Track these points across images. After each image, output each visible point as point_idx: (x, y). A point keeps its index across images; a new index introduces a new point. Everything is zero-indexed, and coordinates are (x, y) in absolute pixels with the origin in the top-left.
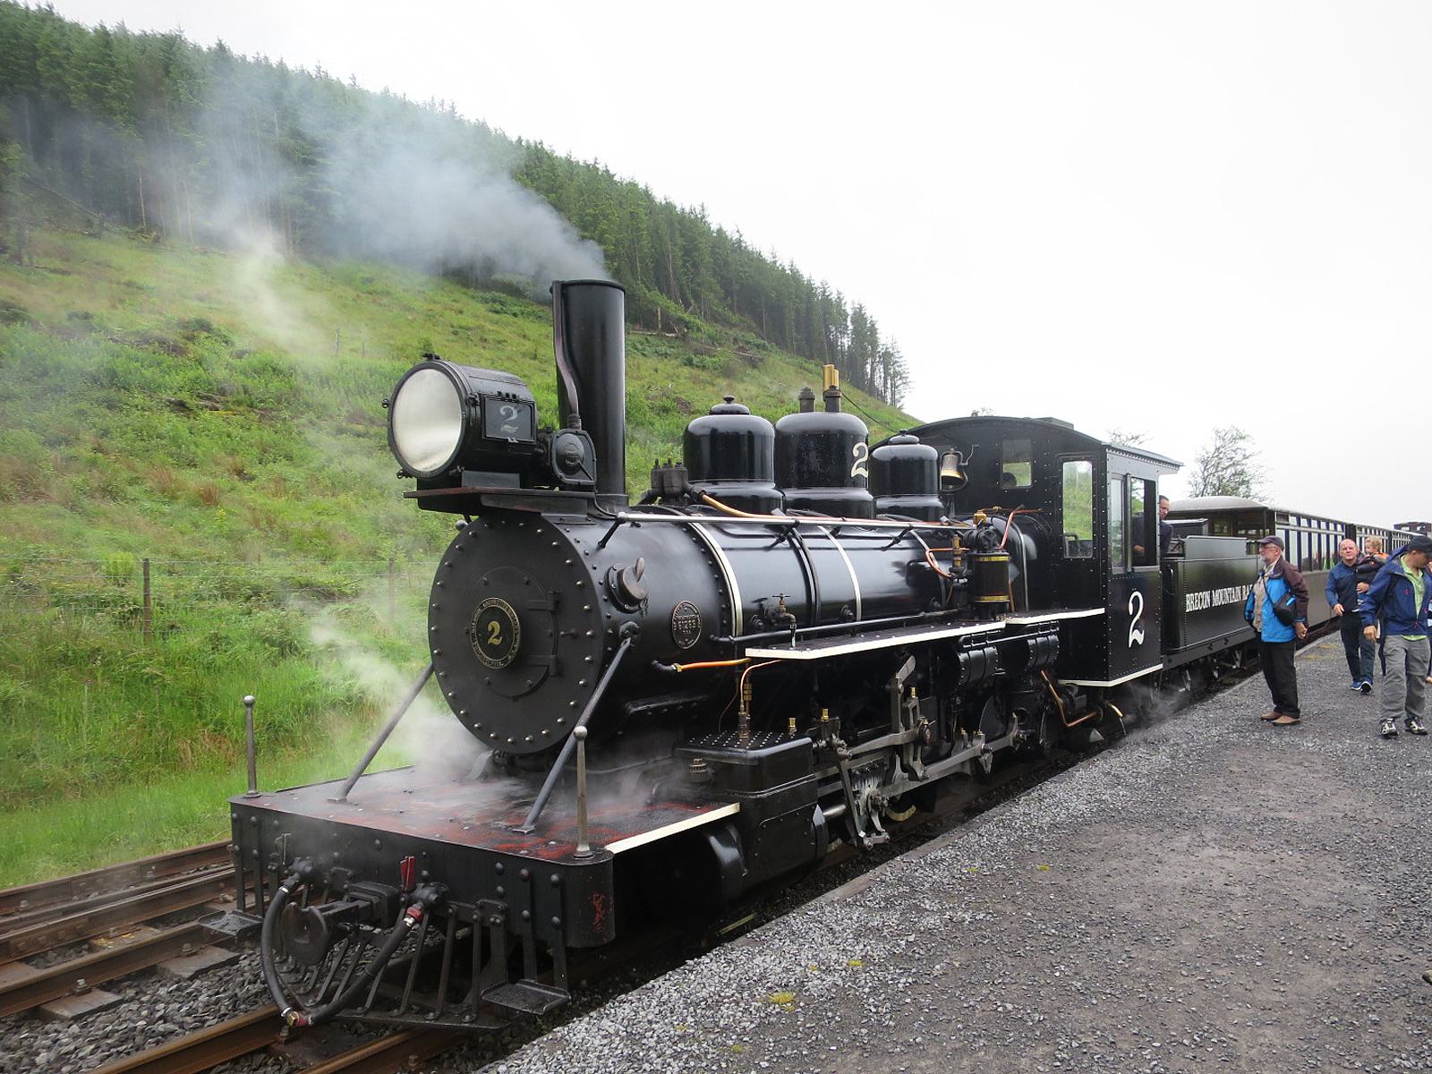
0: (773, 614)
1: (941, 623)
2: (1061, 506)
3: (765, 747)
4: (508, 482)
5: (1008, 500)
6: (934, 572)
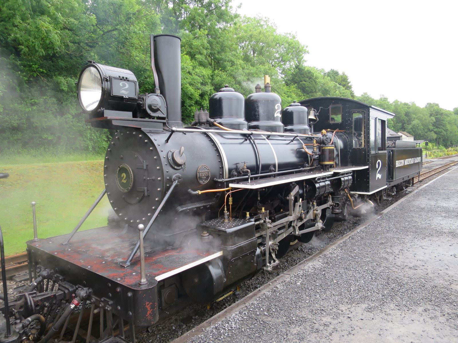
4: (128, 115)
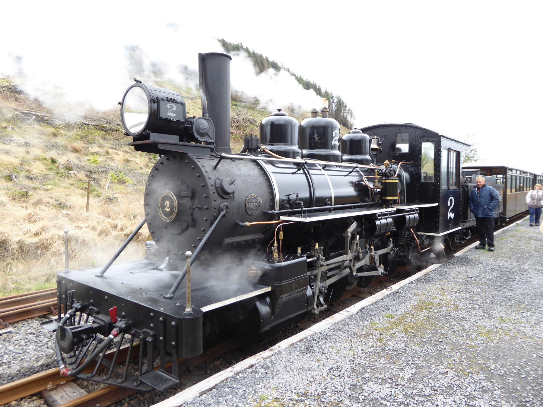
0: (293, 201)
1: (369, 207)
2: (421, 160)
3: (284, 261)
4: (174, 139)
5: (399, 157)
6: (366, 187)
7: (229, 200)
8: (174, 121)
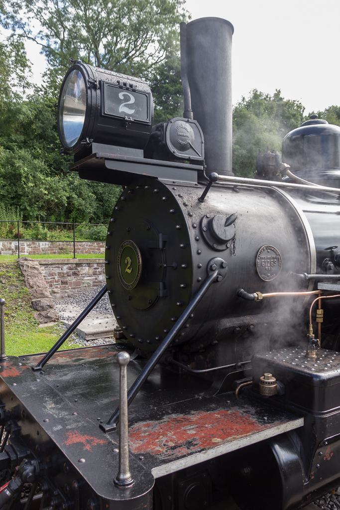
4: (137, 154)
7: (227, 252)
8: (131, 121)
